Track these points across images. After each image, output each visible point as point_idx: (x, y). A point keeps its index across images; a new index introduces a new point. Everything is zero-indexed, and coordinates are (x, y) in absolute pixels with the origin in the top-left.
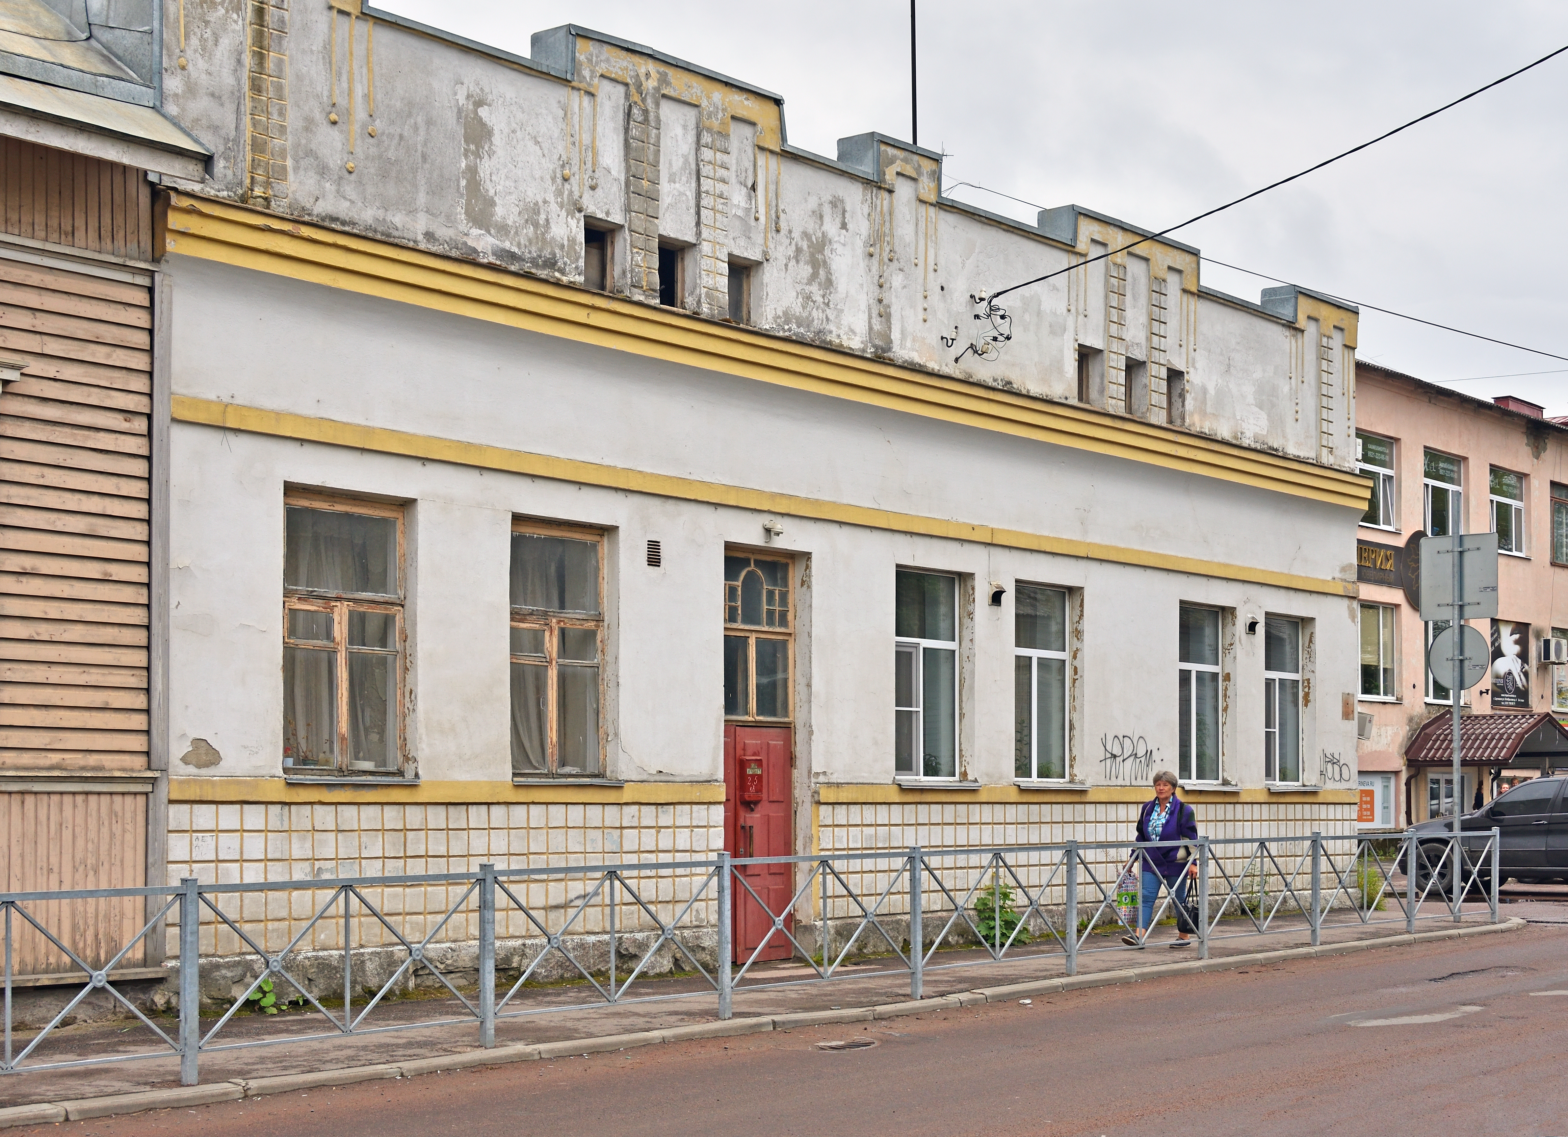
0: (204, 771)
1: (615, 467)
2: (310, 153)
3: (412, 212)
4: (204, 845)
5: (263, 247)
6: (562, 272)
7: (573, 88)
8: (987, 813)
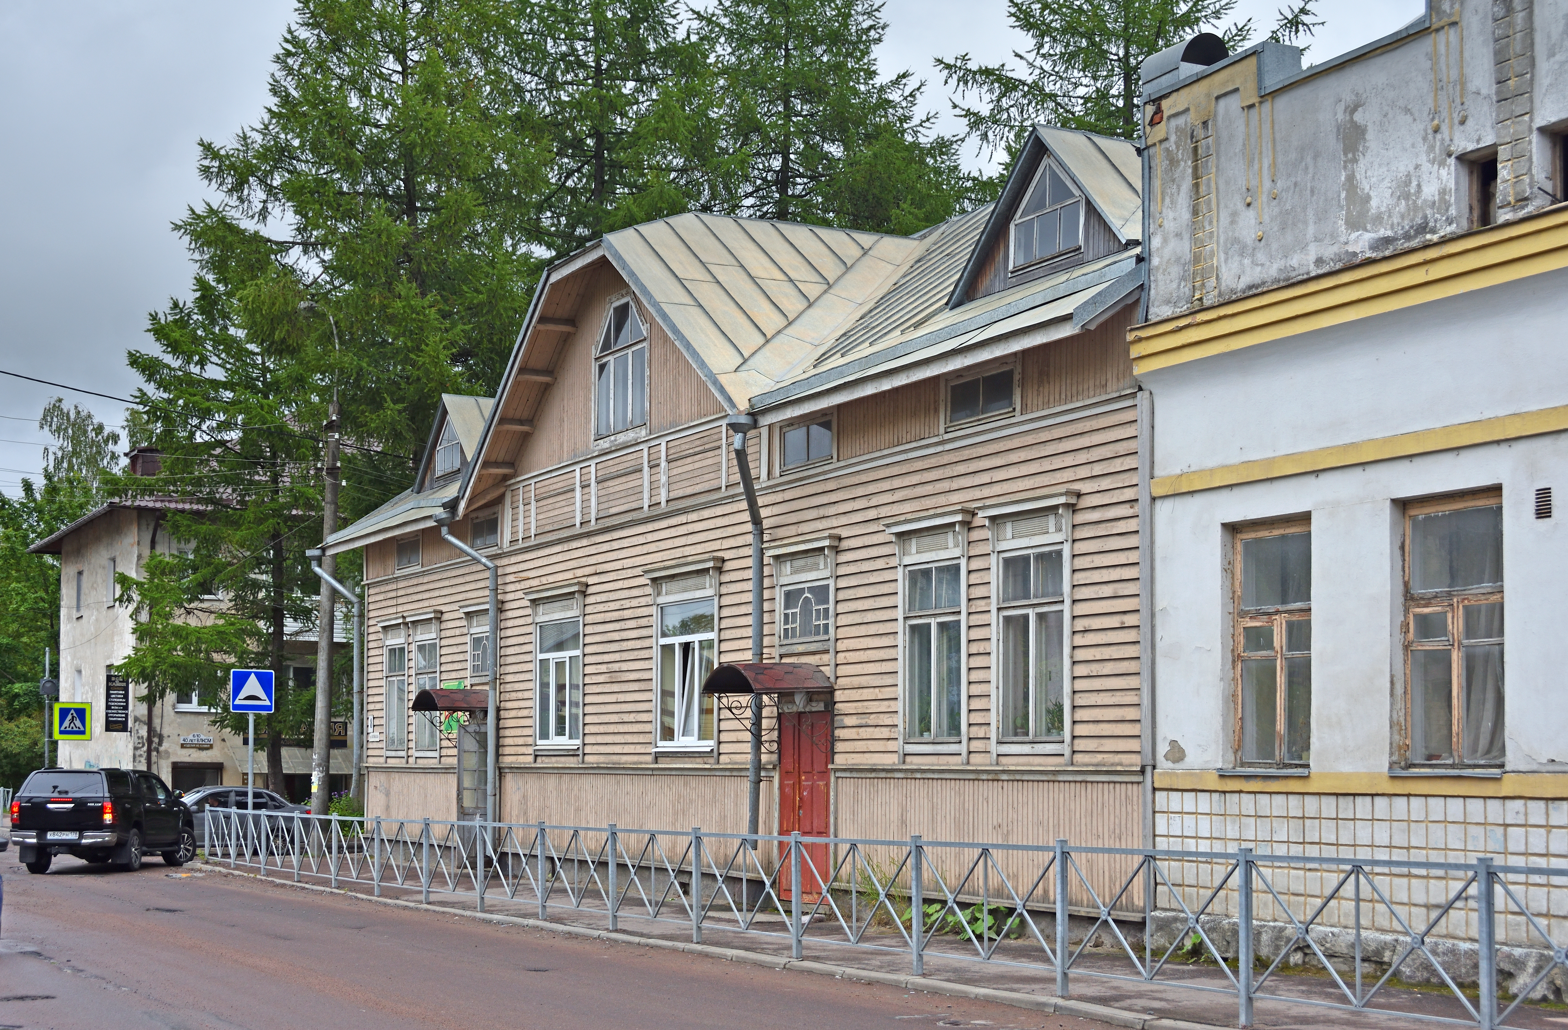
0: (1177, 766)
1: (1497, 418)
2: (1236, 241)
3: (1304, 248)
5: (1179, 344)
6: (1433, 231)
7: (1437, 30)
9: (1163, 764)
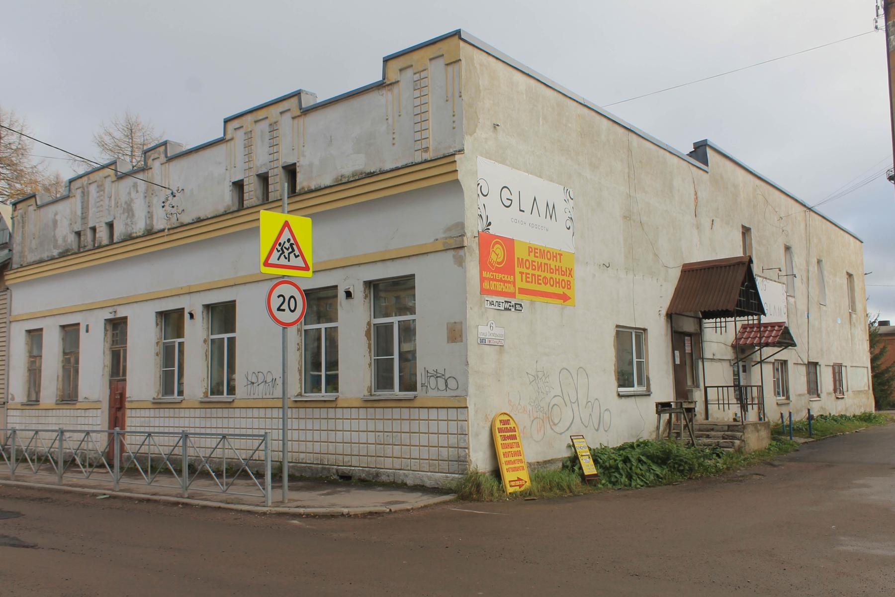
4: (15, 419)
7: (388, 85)
8: (187, 413)
9: (10, 401)
